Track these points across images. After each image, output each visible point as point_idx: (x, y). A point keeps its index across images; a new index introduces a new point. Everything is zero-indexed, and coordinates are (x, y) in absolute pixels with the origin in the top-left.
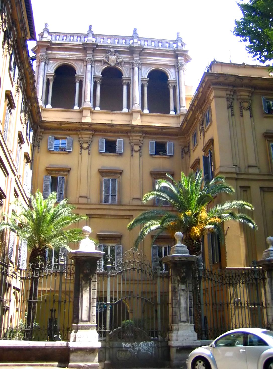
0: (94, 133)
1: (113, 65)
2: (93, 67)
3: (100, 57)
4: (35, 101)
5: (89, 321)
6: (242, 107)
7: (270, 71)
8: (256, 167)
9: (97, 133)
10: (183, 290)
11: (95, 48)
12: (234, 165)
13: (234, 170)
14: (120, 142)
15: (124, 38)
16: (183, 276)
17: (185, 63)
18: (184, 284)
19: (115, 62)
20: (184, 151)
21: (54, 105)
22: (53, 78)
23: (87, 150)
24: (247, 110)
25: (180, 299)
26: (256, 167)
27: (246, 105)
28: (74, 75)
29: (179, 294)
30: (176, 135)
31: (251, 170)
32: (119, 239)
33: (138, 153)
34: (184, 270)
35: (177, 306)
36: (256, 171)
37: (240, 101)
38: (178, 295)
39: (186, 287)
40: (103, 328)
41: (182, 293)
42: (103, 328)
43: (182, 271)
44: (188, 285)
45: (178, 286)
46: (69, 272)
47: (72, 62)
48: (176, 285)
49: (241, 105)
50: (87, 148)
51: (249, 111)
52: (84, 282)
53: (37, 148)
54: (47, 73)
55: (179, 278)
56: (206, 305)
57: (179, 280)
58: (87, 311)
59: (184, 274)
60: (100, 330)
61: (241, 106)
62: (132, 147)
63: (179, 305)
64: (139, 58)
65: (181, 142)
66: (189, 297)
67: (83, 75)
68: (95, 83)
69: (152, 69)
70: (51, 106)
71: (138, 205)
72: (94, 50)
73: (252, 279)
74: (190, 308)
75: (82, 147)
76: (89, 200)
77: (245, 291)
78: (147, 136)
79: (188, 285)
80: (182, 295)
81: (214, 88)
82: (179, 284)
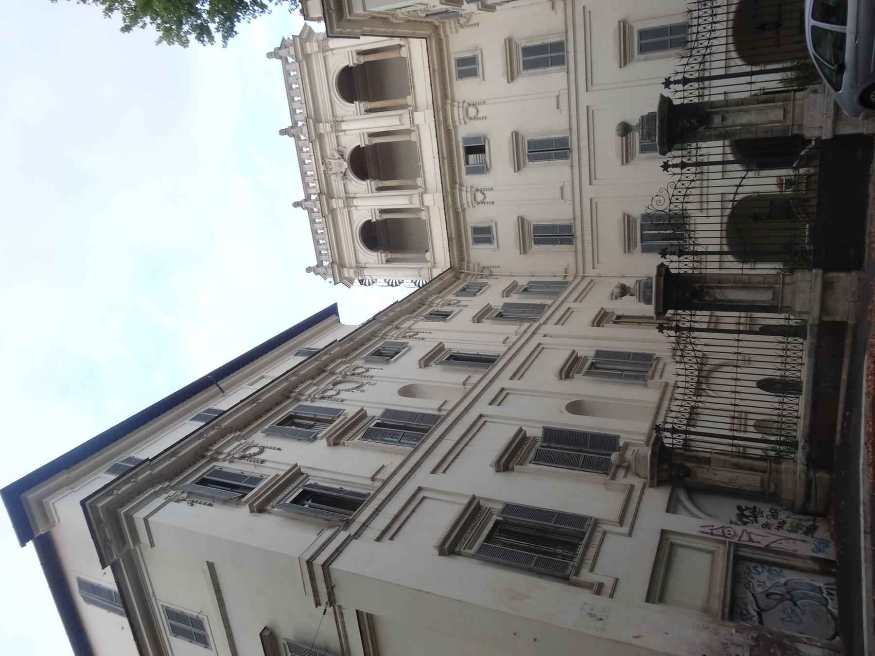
1: (345, 165)
3: (337, 185)
4: (425, 291)
10: (724, 119)
11: (327, 194)
14: (465, 131)
15: (299, 148)
16: (696, 124)
17: (314, 39)
18: (713, 119)
19: (342, 160)
20: (466, 23)
22: (362, 104)
25: (741, 125)
28: (363, 148)
29: (730, 127)
30: (439, 41)
33: (487, 193)
34: (685, 121)
35: (754, 129)
38: (732, 128)
39: (717, 113)
41: (729, 122)
43: (688, 125)
44: (713, 110)
45: (716, 129)
47: (330, 79)
48: (714, 132)
50: (483, 194)
52: (707, 298)
53: (492, 269)
54: (369, 193)
55: (701, 129)
57: (705, 128)
59: (692, 121)
62: (479, 203)
63: (752, 125)
64: (326, 122)
65: (451, 32)
67: (348, 52)
70: (418, 179)
71: (595, 567)
72: (318, 120)
75: (475, 118)
76: (562, 92)
78: (458, 182)
79: (713, 110)
80: (733, 121)
81: (350, 14)
82: (711, 128)
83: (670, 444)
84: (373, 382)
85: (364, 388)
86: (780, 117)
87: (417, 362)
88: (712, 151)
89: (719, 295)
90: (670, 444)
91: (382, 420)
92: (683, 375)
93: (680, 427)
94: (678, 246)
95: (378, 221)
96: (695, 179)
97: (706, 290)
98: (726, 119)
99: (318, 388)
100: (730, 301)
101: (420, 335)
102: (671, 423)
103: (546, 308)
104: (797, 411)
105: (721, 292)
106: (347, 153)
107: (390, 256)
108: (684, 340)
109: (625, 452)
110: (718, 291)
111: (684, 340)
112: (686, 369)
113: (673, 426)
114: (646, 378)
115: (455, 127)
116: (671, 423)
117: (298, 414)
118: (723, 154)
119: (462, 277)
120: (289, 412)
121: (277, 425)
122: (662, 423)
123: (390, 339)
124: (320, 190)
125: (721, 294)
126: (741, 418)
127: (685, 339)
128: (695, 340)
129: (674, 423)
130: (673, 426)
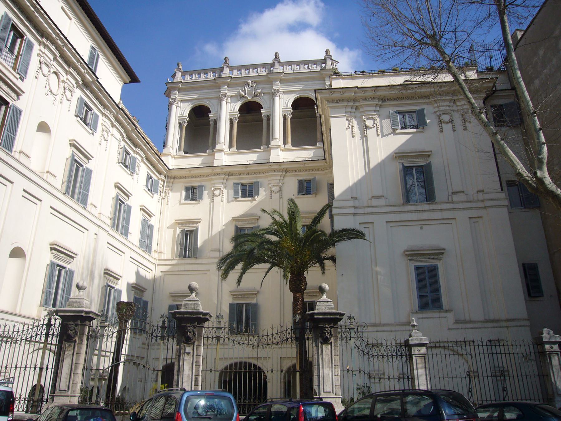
0: (227, 177)
2: (280, 99)
5: (324, 392)
6: (464, 120)
7: (437, 72)
8: (462, 192)
9: (288, 174)
10: (188, 353)
12: (352, 198)
13: (351, 203)
21: (293, 144)
23: (278, 194)
24: (447, 123)
26: (462, 192)
27: (446, 118)
31: (375, 202)
32: (255, 296)
36: (382, 202)
37: (462, 112)
40: (242, 401)
42: (242, 401)
46: (206, 336)
49: (463, 117)
51: (450, 125)
53: (166, 200)
56: (360, 372)
58: (66, 379)
60: (239, 404)
61: (463, 118)
66: (196, 362)
68: (231, 121)
69: (197, 103)
73: (291, 338)
74: (195, 375)
77: (310, 355)
80: (186, 360)
81: (329, 107)
83: (92, 324)
84: (56, 103)
85: (50, 96)
86: (62, 388)
87: (74, 139)
88: (109, 344)
89: (68, 353)
90: (92, 324)
91: (11, 106)
92: (4, 330)
93: (52, 330)
94: (224, 327)
95: (209, 118)
96: (153, 336)
97: (73, 344)
98: (188, 355)
99: (51, 60)
100: (63, 361)
101: (104, 142)
102: (55, 323)
103: (125, 237)
104: (18, 410)
105: (70, 355)
106: (257, 100)
107: (185, 125)
108: (111, 330)
109: (294, 297)
110: (71, 353)
111: (111, 330)
112: (18, 332)
113: (52, 325)
114: (45, 306)
115: (266, 177)
116: (55, 323)
117: (24, 42)
118: (432, 355)
119: (162, 177)
120: (26, 35)
121: (12, 23)
122: (356, 320)
123: (101, 119)
124: (234, 78)
125: (68, 354)
126: (5, 373)
127: (112, 331)
128: (39, 338)
129: (54, 326)
130: (52, 325)
